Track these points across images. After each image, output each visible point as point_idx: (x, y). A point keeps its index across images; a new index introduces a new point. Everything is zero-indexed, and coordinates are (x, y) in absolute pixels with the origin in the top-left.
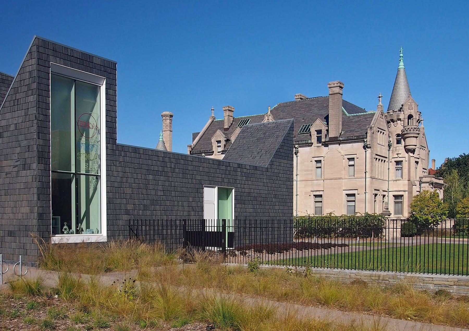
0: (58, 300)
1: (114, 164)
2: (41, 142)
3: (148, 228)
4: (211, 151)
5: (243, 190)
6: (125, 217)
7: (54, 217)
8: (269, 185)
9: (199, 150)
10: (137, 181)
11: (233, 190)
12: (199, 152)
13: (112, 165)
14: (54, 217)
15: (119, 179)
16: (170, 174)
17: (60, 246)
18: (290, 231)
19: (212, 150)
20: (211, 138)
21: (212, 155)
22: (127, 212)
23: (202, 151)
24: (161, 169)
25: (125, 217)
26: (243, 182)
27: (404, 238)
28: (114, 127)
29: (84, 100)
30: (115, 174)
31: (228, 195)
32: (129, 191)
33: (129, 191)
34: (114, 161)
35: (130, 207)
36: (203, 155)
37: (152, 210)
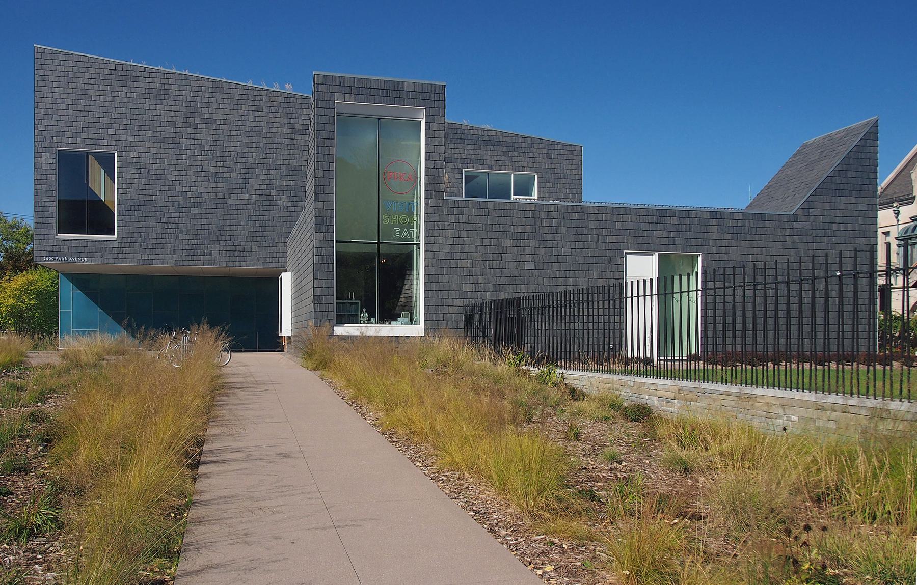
0: (663, 500)
1: (438, 227)
2: (320, 205)
3: (720, 348)
4: (910, 196)
5: (726, 257)
6: (459, 302)
7: (338, 301)
8: (801, 246)
9: (889, 197)
10: (481, 249)
11: (700, 259)
12: (889, 200)
13: (436, 227)
14: (338, 301)
15: (446, 248)
16: (549, 237)
17: (343, 338)
18: (839, 324)
19: (912, 194)
20: (911, 172)
21: (913, 203)
22: (462, 295)
23: (894, 199)
24: (528, 229)
25: (459, 302)
26: (726, 243)
27: (678, 293)
28: (441, 174)
29: (402, 143)
30: (441, 240)
31: (694, 265)
32: (465, 264)
33: (465, 264)
34: (439, 223)
35: (467, 287)
36: (895, 205)
37: (511, 291)
